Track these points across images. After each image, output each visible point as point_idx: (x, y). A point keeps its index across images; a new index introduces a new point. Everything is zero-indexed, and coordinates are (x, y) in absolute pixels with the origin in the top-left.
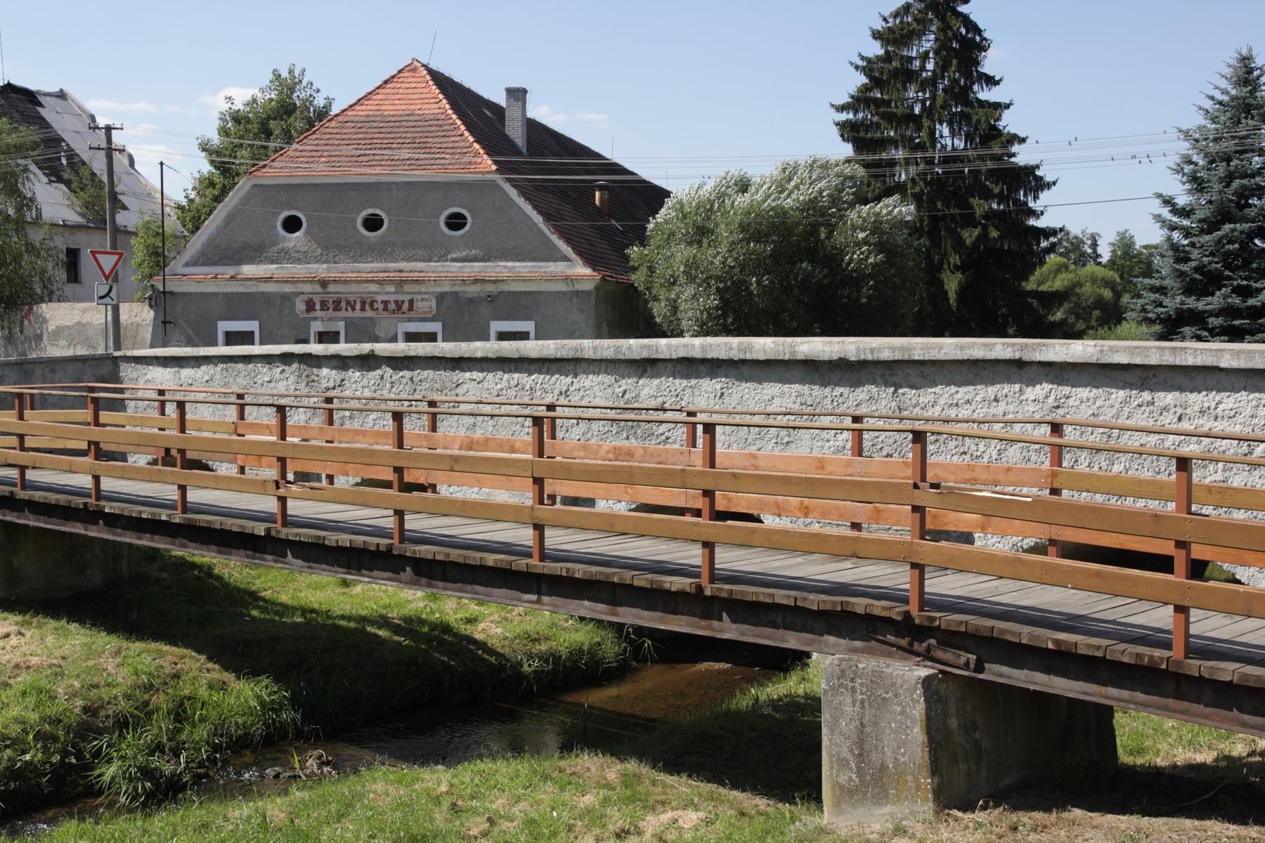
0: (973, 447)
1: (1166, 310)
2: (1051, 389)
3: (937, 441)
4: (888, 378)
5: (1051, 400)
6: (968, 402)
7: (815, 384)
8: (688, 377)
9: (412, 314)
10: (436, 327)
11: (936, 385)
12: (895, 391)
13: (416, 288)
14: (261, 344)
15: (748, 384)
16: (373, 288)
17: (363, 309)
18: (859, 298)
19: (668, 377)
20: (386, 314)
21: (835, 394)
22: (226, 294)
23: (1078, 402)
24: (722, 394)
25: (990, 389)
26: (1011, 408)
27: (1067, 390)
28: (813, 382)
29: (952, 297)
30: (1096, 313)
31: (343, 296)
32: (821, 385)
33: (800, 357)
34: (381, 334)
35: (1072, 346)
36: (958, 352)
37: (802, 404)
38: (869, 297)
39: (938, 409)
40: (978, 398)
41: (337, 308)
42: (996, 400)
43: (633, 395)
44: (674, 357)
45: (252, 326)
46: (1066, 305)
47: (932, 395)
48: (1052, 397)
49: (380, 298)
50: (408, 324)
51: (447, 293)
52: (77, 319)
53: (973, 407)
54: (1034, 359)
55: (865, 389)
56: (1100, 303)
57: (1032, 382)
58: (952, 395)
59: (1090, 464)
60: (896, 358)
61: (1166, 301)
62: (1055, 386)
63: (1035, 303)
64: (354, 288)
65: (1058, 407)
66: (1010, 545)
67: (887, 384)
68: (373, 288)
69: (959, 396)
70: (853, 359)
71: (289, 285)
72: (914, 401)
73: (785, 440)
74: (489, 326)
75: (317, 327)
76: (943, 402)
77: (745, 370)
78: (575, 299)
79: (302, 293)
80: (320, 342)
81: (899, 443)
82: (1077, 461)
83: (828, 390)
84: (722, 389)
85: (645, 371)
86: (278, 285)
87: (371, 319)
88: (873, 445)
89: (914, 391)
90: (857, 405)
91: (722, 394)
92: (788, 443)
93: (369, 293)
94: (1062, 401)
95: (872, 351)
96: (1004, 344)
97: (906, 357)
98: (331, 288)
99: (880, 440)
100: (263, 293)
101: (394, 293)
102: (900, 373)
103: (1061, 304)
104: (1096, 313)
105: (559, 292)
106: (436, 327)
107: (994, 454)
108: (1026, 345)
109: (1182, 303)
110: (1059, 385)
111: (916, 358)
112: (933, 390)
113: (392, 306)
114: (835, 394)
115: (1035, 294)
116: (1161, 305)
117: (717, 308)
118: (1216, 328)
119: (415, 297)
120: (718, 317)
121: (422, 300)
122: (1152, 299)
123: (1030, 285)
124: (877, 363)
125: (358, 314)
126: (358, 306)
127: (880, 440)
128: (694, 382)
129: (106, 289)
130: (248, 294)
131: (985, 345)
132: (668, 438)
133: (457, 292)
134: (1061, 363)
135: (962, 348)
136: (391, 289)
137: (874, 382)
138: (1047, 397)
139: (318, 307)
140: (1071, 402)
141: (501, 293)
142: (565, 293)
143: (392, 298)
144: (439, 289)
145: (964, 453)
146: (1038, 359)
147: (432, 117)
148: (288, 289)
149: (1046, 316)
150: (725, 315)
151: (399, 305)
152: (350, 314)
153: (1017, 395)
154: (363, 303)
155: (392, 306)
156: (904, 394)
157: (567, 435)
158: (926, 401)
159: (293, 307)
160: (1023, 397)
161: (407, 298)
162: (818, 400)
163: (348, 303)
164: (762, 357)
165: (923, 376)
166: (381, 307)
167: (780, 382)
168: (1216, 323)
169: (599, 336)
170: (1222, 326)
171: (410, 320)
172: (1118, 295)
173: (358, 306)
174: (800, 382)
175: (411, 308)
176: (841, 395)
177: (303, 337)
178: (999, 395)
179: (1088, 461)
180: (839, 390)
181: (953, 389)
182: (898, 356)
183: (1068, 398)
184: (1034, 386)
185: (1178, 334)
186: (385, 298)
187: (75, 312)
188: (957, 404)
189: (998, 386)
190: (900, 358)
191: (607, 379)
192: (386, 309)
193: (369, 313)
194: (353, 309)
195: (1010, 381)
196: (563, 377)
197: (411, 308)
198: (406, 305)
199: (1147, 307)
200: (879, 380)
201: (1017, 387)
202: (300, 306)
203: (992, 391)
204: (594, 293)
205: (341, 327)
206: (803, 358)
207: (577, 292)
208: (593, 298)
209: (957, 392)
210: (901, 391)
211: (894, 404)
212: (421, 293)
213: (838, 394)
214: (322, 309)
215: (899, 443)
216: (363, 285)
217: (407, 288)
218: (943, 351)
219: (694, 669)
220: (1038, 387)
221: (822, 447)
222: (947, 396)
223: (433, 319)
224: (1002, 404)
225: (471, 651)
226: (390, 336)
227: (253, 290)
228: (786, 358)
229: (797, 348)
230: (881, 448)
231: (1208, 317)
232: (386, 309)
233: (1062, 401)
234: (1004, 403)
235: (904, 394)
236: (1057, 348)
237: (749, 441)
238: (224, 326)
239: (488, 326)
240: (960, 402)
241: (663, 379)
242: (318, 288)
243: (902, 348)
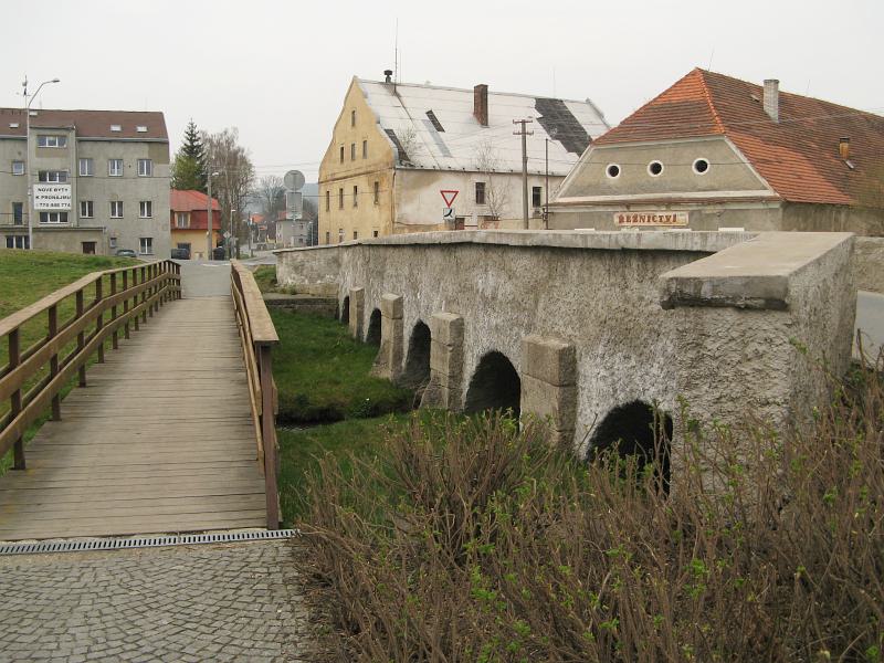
113: (664, 219)
151: (668, 218)
155: (664, 219)
159: (613, 221)
175: (674, 221)
197: (674, 221)
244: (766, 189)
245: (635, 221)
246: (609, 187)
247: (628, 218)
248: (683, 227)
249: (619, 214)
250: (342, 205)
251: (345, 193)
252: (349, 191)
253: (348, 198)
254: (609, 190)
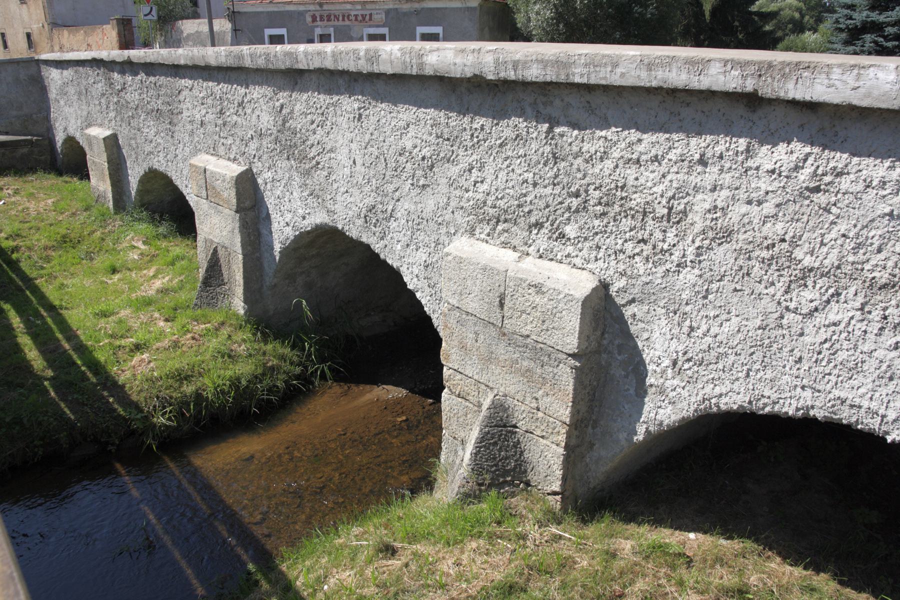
0: (658, 235)
1: (854, 21)
2: (808, 155)
3: (604, 214)
4: (541, 107)
5: (804, 175)
6: (656, 159)
7: (452, 111)
8: (330, 92)
9: (371, 23)
10: (385, 31)
11: (608, 127)
12: (550, 130)
13: (373, 6)
14: (289, 43)
15: (383, 105)
16: (349, 7)
17: (343, 20)
18: (646, 14)
19: (314, 92)
20: (356, 23)
21: (475, 126)
22: (268, 12)
23: (860, 186)
24: (360, 115)
25: (694, 141)
26: (727, 178)
27: (840, 159)
28: (449, 108)
29: (707, 14)
30: (790, 26)
31: (332, 12)
32: (459, 113)
33: (429, 71)
34: (354, 35)
35: (871, 72)
36: (644, 74)
37: (438, 137)
38: (651, 14)
39: (609, 164)
40: (672, 156)
41: (329, 20)
42: (703, 162)
43: (288, 111)
44: (311, 68)
45: (283, 31)
46: (774, 22)
47: (601, 142)
48: (808, 170)
49: (353, 13)
50: (369, 29)
51: (391, 9)
52: (196, 29)
53: (663, 169)
54: (782, 94)
55: (511, 122)
56: (792, 20)
57: (772, 138)
58: (631, 145)
59: (863, 305)
60: (548, 79)
61: (855, 15)
62: (816, 150)
63: (756, 18)
64: (338, 7)
65: (817, 190)
66: (700, 398)
67: (539, 118)
68: (349, 7)
69: (641, 148)
70: (491, 77)
71: (302, 6)
72: (575, 149)
73: (421, 183)
74: (415, 29)
75: (318, 31)
76: (616, 154)
77: (380, 85)
78: (466, 13)
79: (310, 11)
80: (321, 42)
81: (552, 209)
82: (838, 294)
83: (467, 119)
84: (359, 109)
85: (296, 84)
86: (295, 6)
87: (348, 26)
88: (519, 206)
89: (576, 132)
90: (501, 146)
91: (360, 115)
92: (423, 186)
93: (347, 10)
94: (828, 179)
95: (516, 65)
96: (726, 62)
97: (562, 78)
98: (325, 7)
99: (528, 199)
100: (288, 11)
101: (361, 10)
102: (557, 102)
103: (772, 20)
104: (790, 26)
105: (457, 8)
106: (385, 31)
107: (691, 251)
108: (770, 65)
109: (868, 17)
110: (825, 147)
111: (577, 80)
112: (603, 133)
113: (360, 18)
114: (475, 126)
115: (759, 14)
116: (851, 18)
117: (552, 19)
118: (891, 35)
119: (373, 12)
120: (552, 24)
121: (377, 14)
122: (844, 14)
123: (754, 8)
124: (525, 85)
125: (341, 23)
126: (341, 18)
127: (528, 199)
128: (336, 98)
129: (149, 9)
130: (280, 12)
131: (690, 62)
132: (318, 163)
133: (397, 9)
134: (837, 106)
135: (650, 67)
136: (359, 7)
137: (522, 114)
138: (797, 168)
139: (318, 19)
140: (845, 183)
141: (423, 9)
142: (461, 9)
143: (360, 13)
144: (386, 7)
145: (644, 241)
146: (790, 96)
148: (302, 8)
149: (761, 27)
150: (558, 24)
151: (364, 16)
152: (336, 23)
153: (740, 158)
154: (343, 16)
155: (360, 18)
156: (562, 135)
157: (247, 149)
158: (593, 151)
160: (750, 163)
161: (368, 13)
162: (455, 133)
163: (335, 16)
164: (390, 71)
165: (590, 109)
166: (354, 18)
167: (415, 104)
168: (891, 31)
169: (481, 38)
170: (895, 33)
171: (370, 26)
172: (802, 16)
173: (341, 18)
174: (437, 106)
175: (370, 19)
176: (482, 128)
177: (311, 38)
178: (709, 154)
179: (860, 299)
180: (480, 121)
181: (634, 135)
182: (551, 76)
183: (840, 174)
184: (775, 145)
185: (859, 40)
186: (356, 13)
187: (195, 25)
188: (638, 161)
189: (709, 138)
190: (554, 79)
191: (267, 91)
192: (356, 20)
193: (347, 23)
194: (338, 20)
195: (730, 131)
196: (239, 87)
197: (370, 19)
198: (368, 17)
199: (840, 20)
200: (529, 110)
201: (742, 143)
202: (309, 19)
203: (696, 145)
204: (479, 8)
205: (331, 31)
206: (432, 73)
207: (468, 8)
208: (478, 12)
209: (640, 141)
210: (558, 130)
211: (548, 149)
212: (376, 9)
213: (478, 126)
214: (321, 21)
215: (552, 209)
216: (343, 5)
217: (368, 7)
218: (619, 70)
219: (368, 397)
220: (782, 147)
221: (461, 198)
222: (623, 146)
223: (383, 26)
224: (714, 169)
225: (103, 397)
226: (359, 36)
227: (282, 9)
228: (414, 73)
229: (425, 58)
230: (530, 212)
231: (886, 27)
232: (356, 20)
233: (828, 179)
234: (716, 169)
235: (562, 135)
236: (836, 74)
237: (387, 178)
238: (268, 32)
239: (415, 29)
240: (644, 157)
241: (310, 93)
242: (318, 8)
243: (558, 63)
248: (378, 26)
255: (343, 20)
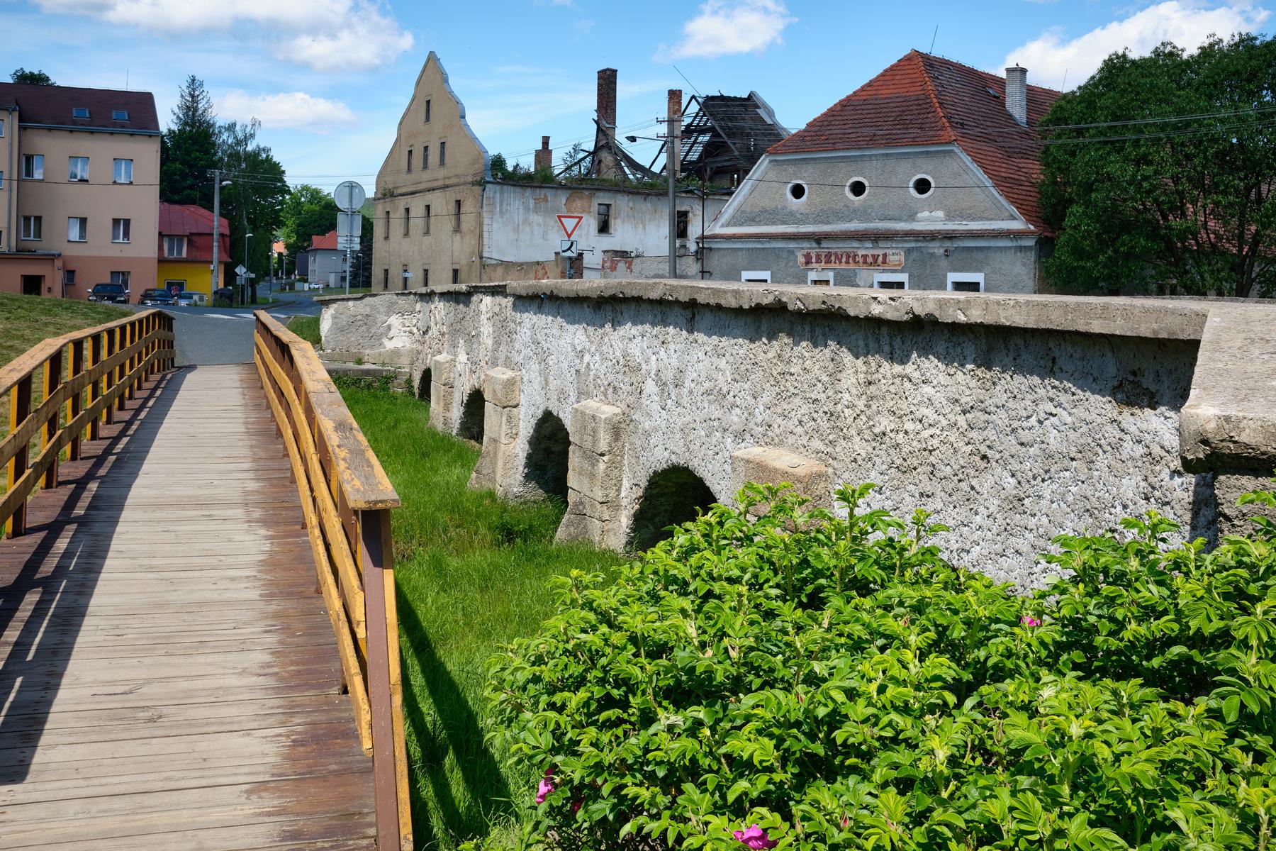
17: (847, 262)
49: (861, 252)
113: (870, 260)
121: (893, 254)
126: (844, 260)
139: (814, 260)
143: (870, 252)
147: (913, 98)
154: (848, 257)
155: (870, 260)
163: (836, 255)
166: (861, 260)
171: (884, 271)
173: (844, 260)
175: (884, 262)
192: (865, 262)
193: (852, 266)
194: (841, 262)
197: (884, 262)
198: (880, 259)
202: (801, 259)
223: (902, 271)
239: (945, 277)
244: (1015, 219)
245: (828, 262)
246: (791, 214)
247: (818, 256)
249: (805, 252)
250: (407, 234)
251: (412, 214)
252: (417, 211)
253: (417, 222)
254: (789, 217)
255: (847, 262)
